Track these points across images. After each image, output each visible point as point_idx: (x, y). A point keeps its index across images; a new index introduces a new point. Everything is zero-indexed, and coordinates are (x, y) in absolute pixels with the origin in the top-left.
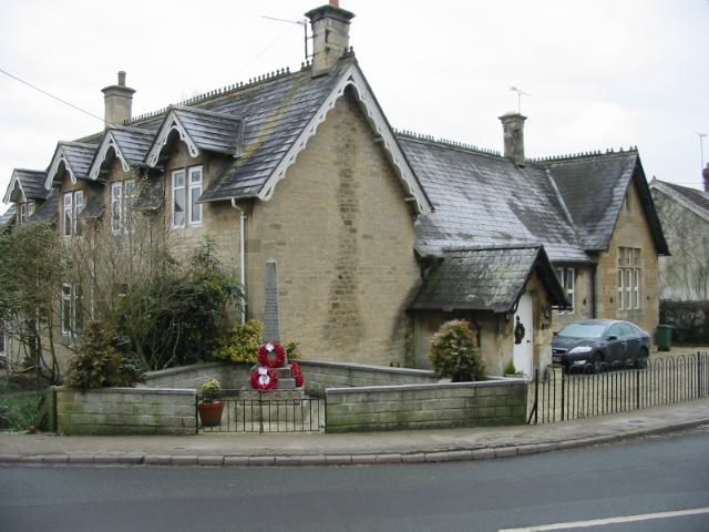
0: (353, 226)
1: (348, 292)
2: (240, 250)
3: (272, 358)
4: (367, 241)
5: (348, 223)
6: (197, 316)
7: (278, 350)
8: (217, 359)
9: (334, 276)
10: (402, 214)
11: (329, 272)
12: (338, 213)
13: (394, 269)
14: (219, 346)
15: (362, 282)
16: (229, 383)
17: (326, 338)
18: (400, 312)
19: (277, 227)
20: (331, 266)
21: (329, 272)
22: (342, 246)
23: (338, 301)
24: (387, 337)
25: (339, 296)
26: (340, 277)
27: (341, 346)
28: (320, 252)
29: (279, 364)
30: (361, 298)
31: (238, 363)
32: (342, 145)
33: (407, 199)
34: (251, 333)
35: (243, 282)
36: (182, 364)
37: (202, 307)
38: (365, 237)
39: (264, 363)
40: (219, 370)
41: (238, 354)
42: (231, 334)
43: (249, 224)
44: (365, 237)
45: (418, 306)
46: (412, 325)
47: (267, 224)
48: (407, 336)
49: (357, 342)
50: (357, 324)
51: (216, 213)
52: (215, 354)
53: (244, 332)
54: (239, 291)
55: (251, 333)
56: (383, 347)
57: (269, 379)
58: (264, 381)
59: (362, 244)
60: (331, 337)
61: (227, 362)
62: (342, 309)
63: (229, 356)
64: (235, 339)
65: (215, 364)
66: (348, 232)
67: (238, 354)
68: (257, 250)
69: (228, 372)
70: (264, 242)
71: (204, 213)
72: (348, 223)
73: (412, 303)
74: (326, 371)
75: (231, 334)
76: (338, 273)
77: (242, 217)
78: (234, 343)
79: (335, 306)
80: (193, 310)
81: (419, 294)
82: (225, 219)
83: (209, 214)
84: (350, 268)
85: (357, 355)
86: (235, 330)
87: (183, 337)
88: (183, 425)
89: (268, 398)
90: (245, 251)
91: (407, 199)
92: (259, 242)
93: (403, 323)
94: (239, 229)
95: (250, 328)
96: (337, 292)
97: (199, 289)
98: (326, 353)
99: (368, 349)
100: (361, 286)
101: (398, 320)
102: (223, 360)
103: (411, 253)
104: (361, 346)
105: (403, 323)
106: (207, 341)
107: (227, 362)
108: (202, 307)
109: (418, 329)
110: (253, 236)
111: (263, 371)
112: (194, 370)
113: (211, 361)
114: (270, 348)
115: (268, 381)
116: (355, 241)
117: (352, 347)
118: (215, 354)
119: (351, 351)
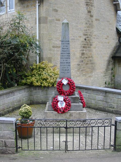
0: (92, 14)
1: (89, 47)
2: (36, 23)
3: (66, 89)
4: (98, 22)
5: (89, 12)
6: (14, 60)
7: (71, 84)
8: (25, 84)
9: (82, 39)
10: (112, 9)
11: (80, 37)
12: (85, 6)
13: (108, 37)
14: (26, 76)
15: (95, 42)
16: (32, 97)
17: (78, 70)
18: (110, 57)
19: (56, 11)
20: (81, 34)
21: (80, 37)
22: (87, 23)
23: (84, 52)
24: (104, 70)
25: (84, 49)
26: (85, 40)
27: (85, 74)
28: (77, 26)
29: (71, 93)
30: (94, 50)
31: (38, 86)
32: (34, 38)
33: (114, 3)
34: (44, 69)
35: (38, 38)
36: (5, 88)
37: (16, 54)
38: (96, 20)
39: (61, 92)
40: (26, 90)
41: (37, 81)
42: (32, 70)
43: (41, 8)
44: (96, 20)
45: (118, 55)
46: (114, 64)
47: (51, 8)
48: (112, 69)
49: (91, 72)
50: (92, 64)
51: (22, 4)
52: (24, 81)
53: (40, 68)
54: (36, 44)
55: (44, 69)
56: (103, 75)
57: (64, 103)
58: (61, 105)
59: (95, 23)
60: (81, 70)
61: (31, 85)
62: (86, 56)
63: (32, 83)
64: (35, 72)
65: (24, 87)
66: (89, 16)
67: (37, 81)
68: (46, 22)
69: (31, 91)
70: (49, 18)
71: (16, 4)
72: (89, 12)
73: (116, 53)
74: (89, 91)
75: (32, 70)
76: (84, 37)
77: (37, 4)
78: (34, 74)
79: (83, 54)
80: (11, 56)
81: (118, 49)
82: (28, 6)
83: (18, 4)
84: (90, 35)
85: (92, 79)
86: (34, 67)
87: (5, 72)
88: (6, 145)
89: (73, 126)
90: (39, 23)
91: (114, 3)
92: (46, 18)
93: (111, 63)
94: (36, 11)
95: (43, 66)
96: (84, 47)
97: (14, 42)
98: (78, 78)
99: (96, 76)
100: (94, 45)
101: (109, 61)
102: (28, 85)
103: (115, 27)
104: (93, 74)
105: (111, 63)
106: (20, 74)
107: (31, 85)
108: (16, 54)
109: (117, 65)
110: (43, 15)
111: (61, 98)
112: (12, 92)
113: (22, 85)
114: (65, 82)
115: (64, 105)
116: (92, 22)
117: (90, 75)
118: (24, 81)
119: (89, 77)
